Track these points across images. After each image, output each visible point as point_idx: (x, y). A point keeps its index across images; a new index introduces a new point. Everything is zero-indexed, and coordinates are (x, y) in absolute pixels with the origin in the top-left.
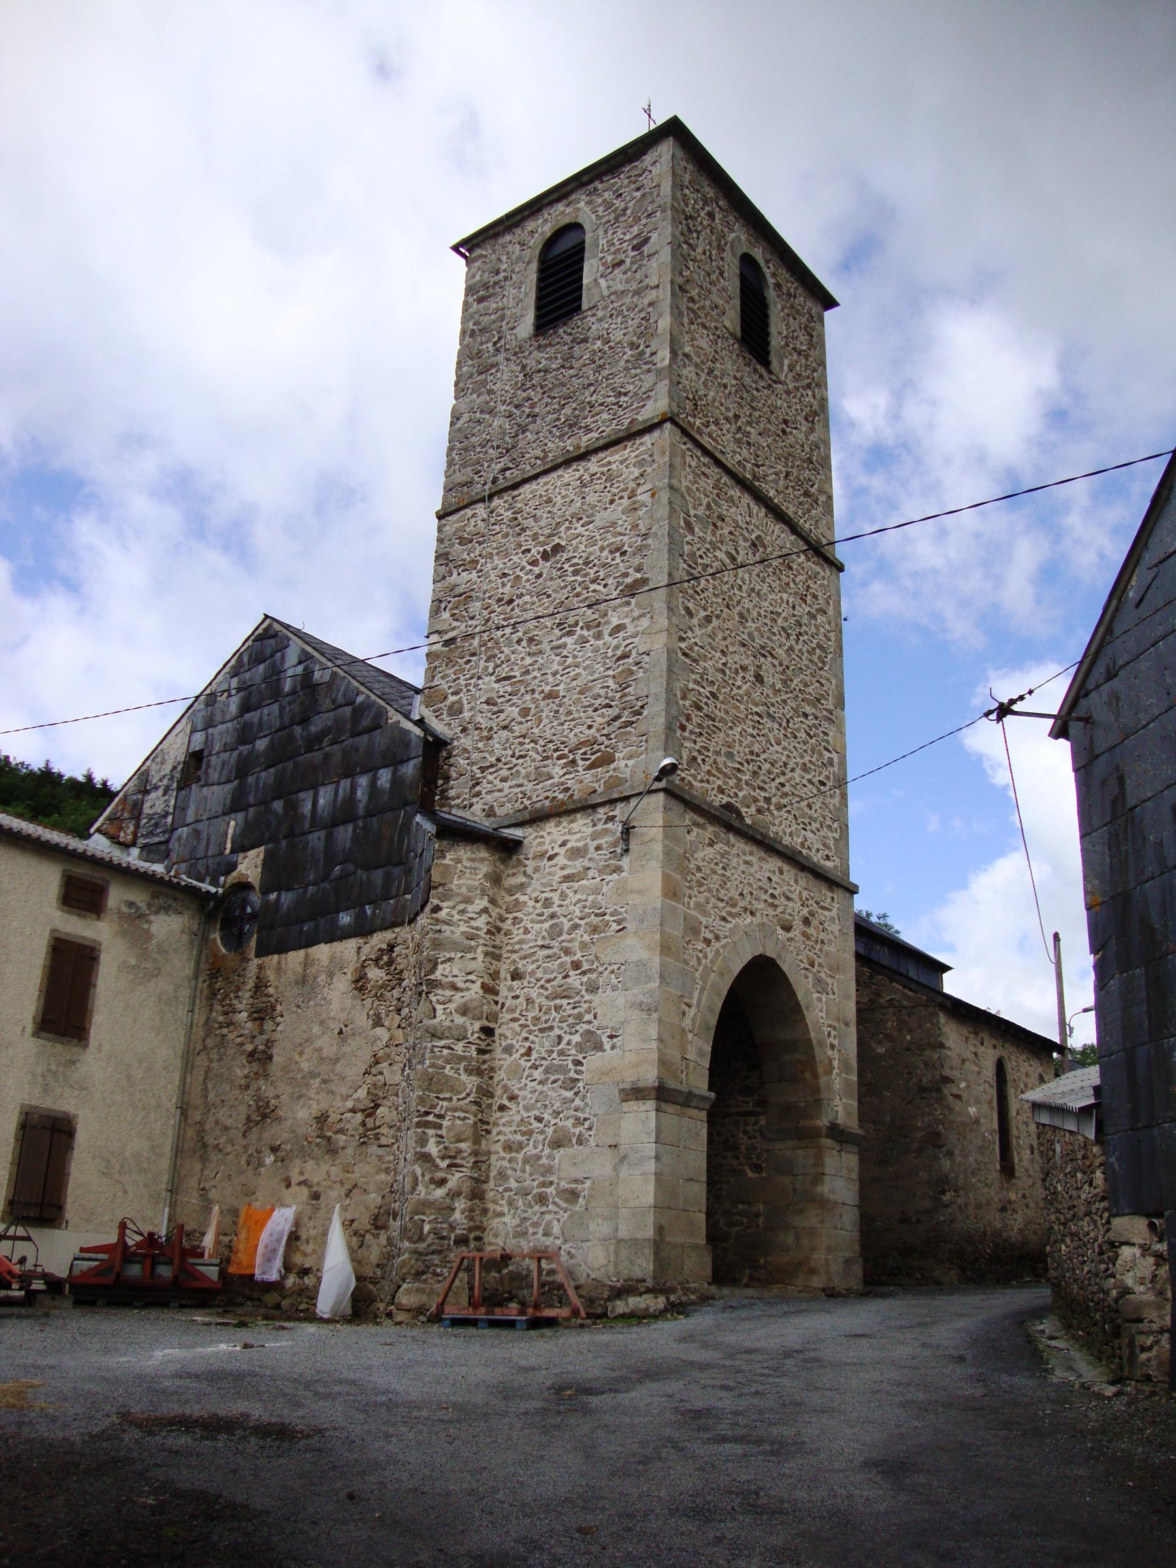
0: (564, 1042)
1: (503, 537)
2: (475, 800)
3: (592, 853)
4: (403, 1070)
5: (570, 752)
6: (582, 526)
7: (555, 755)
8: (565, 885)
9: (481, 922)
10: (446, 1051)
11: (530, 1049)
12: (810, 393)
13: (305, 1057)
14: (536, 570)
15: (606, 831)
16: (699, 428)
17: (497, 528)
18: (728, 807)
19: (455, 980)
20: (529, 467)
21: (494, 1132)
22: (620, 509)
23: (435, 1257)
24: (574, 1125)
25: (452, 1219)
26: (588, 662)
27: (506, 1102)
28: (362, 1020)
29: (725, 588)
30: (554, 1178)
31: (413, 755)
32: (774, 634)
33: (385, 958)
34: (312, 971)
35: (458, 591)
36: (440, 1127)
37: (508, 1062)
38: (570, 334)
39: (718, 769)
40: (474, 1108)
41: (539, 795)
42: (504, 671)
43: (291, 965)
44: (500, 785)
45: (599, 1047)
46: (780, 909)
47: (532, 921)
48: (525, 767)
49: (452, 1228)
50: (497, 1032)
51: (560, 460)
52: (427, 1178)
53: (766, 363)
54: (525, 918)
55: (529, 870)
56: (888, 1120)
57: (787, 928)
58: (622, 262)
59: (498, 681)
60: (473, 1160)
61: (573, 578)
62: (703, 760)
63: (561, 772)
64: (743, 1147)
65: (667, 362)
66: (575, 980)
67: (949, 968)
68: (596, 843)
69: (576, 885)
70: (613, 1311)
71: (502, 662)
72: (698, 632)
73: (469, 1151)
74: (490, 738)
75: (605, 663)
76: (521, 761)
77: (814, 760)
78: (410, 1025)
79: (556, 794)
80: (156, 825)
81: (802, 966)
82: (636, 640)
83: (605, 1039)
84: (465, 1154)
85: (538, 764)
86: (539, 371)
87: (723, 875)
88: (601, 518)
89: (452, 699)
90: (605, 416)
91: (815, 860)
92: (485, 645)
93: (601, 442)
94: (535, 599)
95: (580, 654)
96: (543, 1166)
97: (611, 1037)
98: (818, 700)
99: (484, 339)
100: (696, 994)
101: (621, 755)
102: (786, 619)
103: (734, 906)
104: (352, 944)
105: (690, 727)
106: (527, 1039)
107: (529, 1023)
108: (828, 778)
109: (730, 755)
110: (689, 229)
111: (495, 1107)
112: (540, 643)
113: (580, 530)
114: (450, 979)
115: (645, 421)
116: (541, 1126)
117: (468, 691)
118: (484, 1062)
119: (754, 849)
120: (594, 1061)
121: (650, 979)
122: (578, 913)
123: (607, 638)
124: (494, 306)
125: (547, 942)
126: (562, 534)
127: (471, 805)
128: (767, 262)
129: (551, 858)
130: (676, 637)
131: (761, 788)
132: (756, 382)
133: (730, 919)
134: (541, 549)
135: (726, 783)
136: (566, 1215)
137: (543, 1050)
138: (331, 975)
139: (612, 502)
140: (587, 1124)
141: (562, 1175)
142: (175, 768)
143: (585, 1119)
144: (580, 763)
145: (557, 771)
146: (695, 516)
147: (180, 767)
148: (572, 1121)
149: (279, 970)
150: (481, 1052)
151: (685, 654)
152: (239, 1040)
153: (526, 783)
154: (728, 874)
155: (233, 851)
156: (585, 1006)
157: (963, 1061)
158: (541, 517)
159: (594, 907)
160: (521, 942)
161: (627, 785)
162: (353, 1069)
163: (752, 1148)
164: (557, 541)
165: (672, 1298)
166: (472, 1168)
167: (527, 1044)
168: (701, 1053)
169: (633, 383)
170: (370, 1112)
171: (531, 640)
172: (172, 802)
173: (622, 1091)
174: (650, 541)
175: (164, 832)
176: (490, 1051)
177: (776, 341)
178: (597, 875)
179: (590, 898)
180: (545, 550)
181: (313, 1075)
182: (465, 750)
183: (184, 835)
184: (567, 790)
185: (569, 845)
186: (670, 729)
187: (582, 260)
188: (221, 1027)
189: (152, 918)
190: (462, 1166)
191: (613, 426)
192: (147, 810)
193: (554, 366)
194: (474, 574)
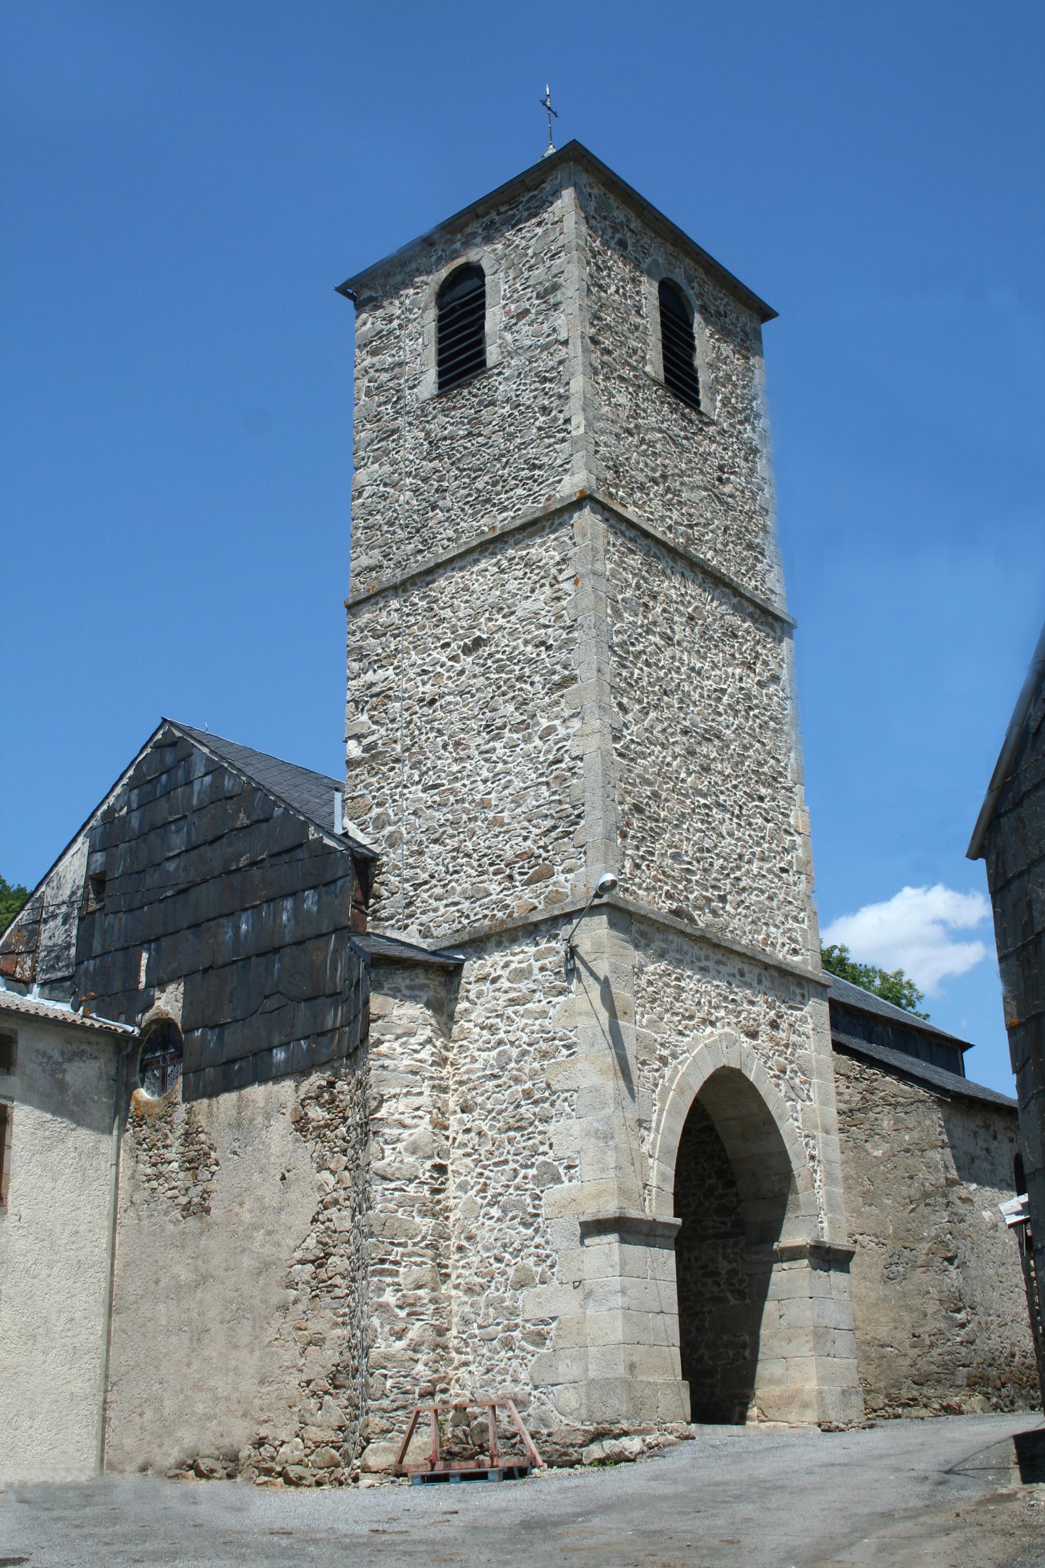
0: (521, 1175)
1: (419, 629)
2: (409, 921)
3: (537, 975)
4: (353, 1216)
5: (506, 866)
6: (503, 617)
7: (492, 869)
8: (511, 1009)
9: (425, 1054)
10: (397, 1194)
11: (485, 1184)
12: (749, 428)
13: (246, 1206)
14: (458, 667)
15: (550, 950)
16: (622, 498)
17: (412, 619)
18: (677, 913)
19: (402, 1117)
20: (441, 551)
21: (454, 1277)
22: (542, 597)
23: (399, 1413)
24: (536, 1265)
25: (414, 1372)
26: (518, 768)
27: (465, 1243)
28: (306, 1167)
29: (662, 673)
30: (519, 1320)
31: (340, 874)
32: (720, 714)
33: (326, 1096)
34: (247, 1113)
35: (376, 690)
36: (396, 1274)
37: (464, 1200)
38: (475, 396)
39: (664, 873)
40: (430, 1252)
41: (479, 916)
42: (431, 779)
43: (222, 1109)
44: (435, 904)
45: (557, 1179)
46: (744, 1015)
47: (479, 1050)
48: (462, 884)
49: (416, 1380)
50: (450, 1168)
51: (475, 543)
52: (387, 1328)
53: (694, 403)
54: (471, 1046)
55: (472, 996)
56: (891, 1231)
57: (753, 1035)
58: (527, 312)
59: (424, 791)
60: (433, 1307)
61: (497, 676)
62: (648, 866)
63: (499, 889)
64: (724, 1272)
65: (582, 430)
66: (527, 1110)
67: (970, 1046)
68: (539, 964)
69: (521, 1009)
70: (587, 1457)
71: (429, 769)
72: (634, 728)
73: (428, 1297)
74: (421, 853)
75: (537, 769)
76: (456, 876)
77: (774, 846)
78: (358, 1166)
79: (495, 912)
80: (58, 958)
81: (772, 1073)
82: (568, 743)
83: (561, 1170)
84: (425, 1301)
85: (474, 880)
86: (445, 439)
87: (678, 987)
88: (525, 607)
89: (376, 811)
90: (520, 491)
91: (780, 956)
92: (408, 750)
93: (518, 523)
94: (458, 698)
95: (510, 759)
96: (507, 1308)
97: (569, 1167)
98: (775, 779)
99: (383, 399)
100: (655, 1117)
101: (560, 868)
102: (731, 696)
103: (691, 1017)
104: (289, 1084)
105: (632, 832)
106: (481, 1174)
107: (482, 1158)
108: (790, 863)
109: (676, 857)
110: (598, 267)
111: (453, 1249)
112: (468, 747)
113: (501, 621)
114: (397, 1116)
115: (562, 498)
116: (502, 1266)
117: (395, 801)
118: (439, 1202)
119: (710, 952)
120: (554, 1193)
121: (604, 1104)
122: (525, 1038)
123: (538, 742)
124: (390, 360)
125: (496, 1071)
126: (483, 627)
127: (406, 927)
128: (690, 281)
129: (494, 981)
130: (610, 737)
131: (714, 887)
132: (684, 429)
133: (687, 1032)
134: (462, 643)
135: (675, 887)
136: (534, 1359)
137: (498, 1186)
138: (268, 1117)
139: (533, 591)
140: (549, 1263)
141: (527, 1316)
142: (73, 893)
143: (548, 1256)
144: (517, 877)
145: (494, 888)
146: (623, 600)
147: (80, 892)
148: (533, 1259)
149: (210, 1114)
150: (436, 1191)
151: (620, 755)
152: (170, 1193)
153: (463, 900)
154: (683, 984)
155: (149, 985)
156: (539, 1138)
157: (972, 1160)
158: (459, 606)
159: (543, 1031)
160: (469, 1071)
161: (569, 900)
162: (299, 1218)
163: (732, 1272)
164: (478, 633)
165: (649, 1439)
166: (433, 1314)
167: (482, 1180)
168: (662, 1176)
169: (547, 455)
170: (320, 1263)
171: (457, 744)
172: (74, 932)
173: (582, 1224)
174: (576, 634)
175: (67, 966)
176: (443, 1190)
177: (704, 377)
178: (542, 998)
179: (537, 1022)
180: (465, 644)
181: (256, 1227)
182: (396, 867)
183: (91, 968)
184: (507, 906)
185: (513, 966)
186: (609, 838)
187: (483, 307)
188: (149, 1181)
189: (66, 1066)
190: (423, 1314)
191: (529, 504)
192: (44, 940)
193: (461, 433)
194: (391, 672)
